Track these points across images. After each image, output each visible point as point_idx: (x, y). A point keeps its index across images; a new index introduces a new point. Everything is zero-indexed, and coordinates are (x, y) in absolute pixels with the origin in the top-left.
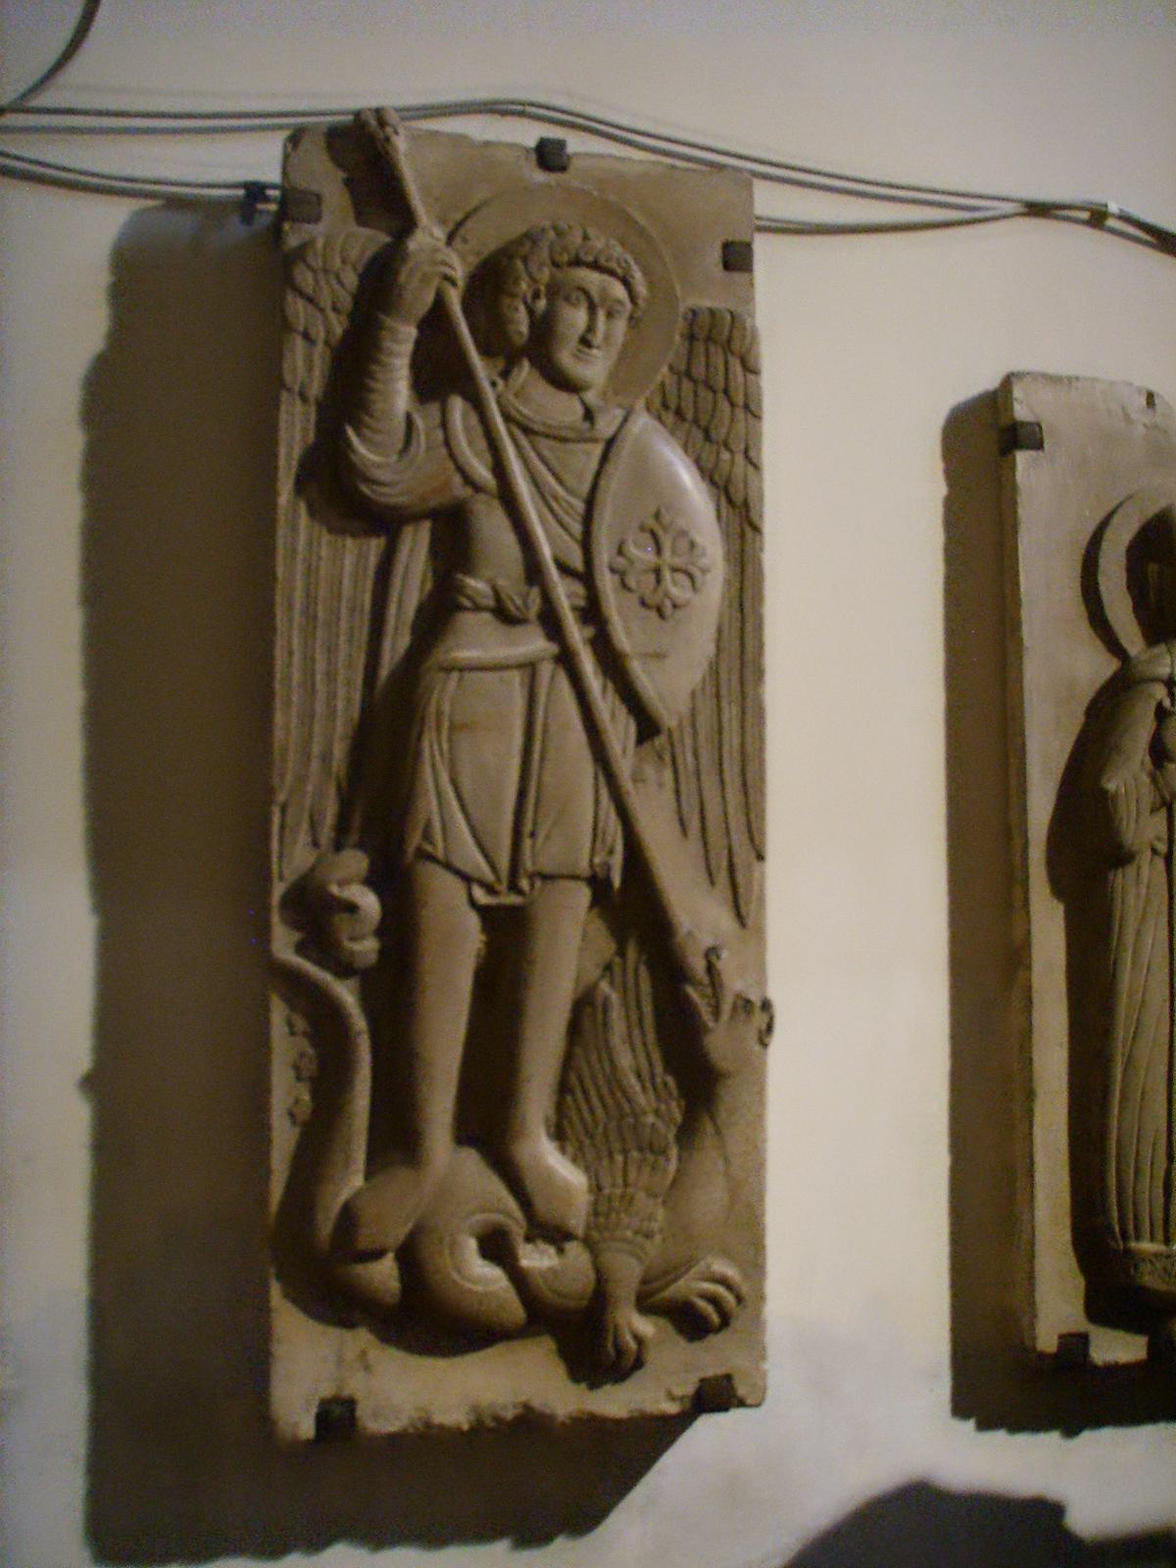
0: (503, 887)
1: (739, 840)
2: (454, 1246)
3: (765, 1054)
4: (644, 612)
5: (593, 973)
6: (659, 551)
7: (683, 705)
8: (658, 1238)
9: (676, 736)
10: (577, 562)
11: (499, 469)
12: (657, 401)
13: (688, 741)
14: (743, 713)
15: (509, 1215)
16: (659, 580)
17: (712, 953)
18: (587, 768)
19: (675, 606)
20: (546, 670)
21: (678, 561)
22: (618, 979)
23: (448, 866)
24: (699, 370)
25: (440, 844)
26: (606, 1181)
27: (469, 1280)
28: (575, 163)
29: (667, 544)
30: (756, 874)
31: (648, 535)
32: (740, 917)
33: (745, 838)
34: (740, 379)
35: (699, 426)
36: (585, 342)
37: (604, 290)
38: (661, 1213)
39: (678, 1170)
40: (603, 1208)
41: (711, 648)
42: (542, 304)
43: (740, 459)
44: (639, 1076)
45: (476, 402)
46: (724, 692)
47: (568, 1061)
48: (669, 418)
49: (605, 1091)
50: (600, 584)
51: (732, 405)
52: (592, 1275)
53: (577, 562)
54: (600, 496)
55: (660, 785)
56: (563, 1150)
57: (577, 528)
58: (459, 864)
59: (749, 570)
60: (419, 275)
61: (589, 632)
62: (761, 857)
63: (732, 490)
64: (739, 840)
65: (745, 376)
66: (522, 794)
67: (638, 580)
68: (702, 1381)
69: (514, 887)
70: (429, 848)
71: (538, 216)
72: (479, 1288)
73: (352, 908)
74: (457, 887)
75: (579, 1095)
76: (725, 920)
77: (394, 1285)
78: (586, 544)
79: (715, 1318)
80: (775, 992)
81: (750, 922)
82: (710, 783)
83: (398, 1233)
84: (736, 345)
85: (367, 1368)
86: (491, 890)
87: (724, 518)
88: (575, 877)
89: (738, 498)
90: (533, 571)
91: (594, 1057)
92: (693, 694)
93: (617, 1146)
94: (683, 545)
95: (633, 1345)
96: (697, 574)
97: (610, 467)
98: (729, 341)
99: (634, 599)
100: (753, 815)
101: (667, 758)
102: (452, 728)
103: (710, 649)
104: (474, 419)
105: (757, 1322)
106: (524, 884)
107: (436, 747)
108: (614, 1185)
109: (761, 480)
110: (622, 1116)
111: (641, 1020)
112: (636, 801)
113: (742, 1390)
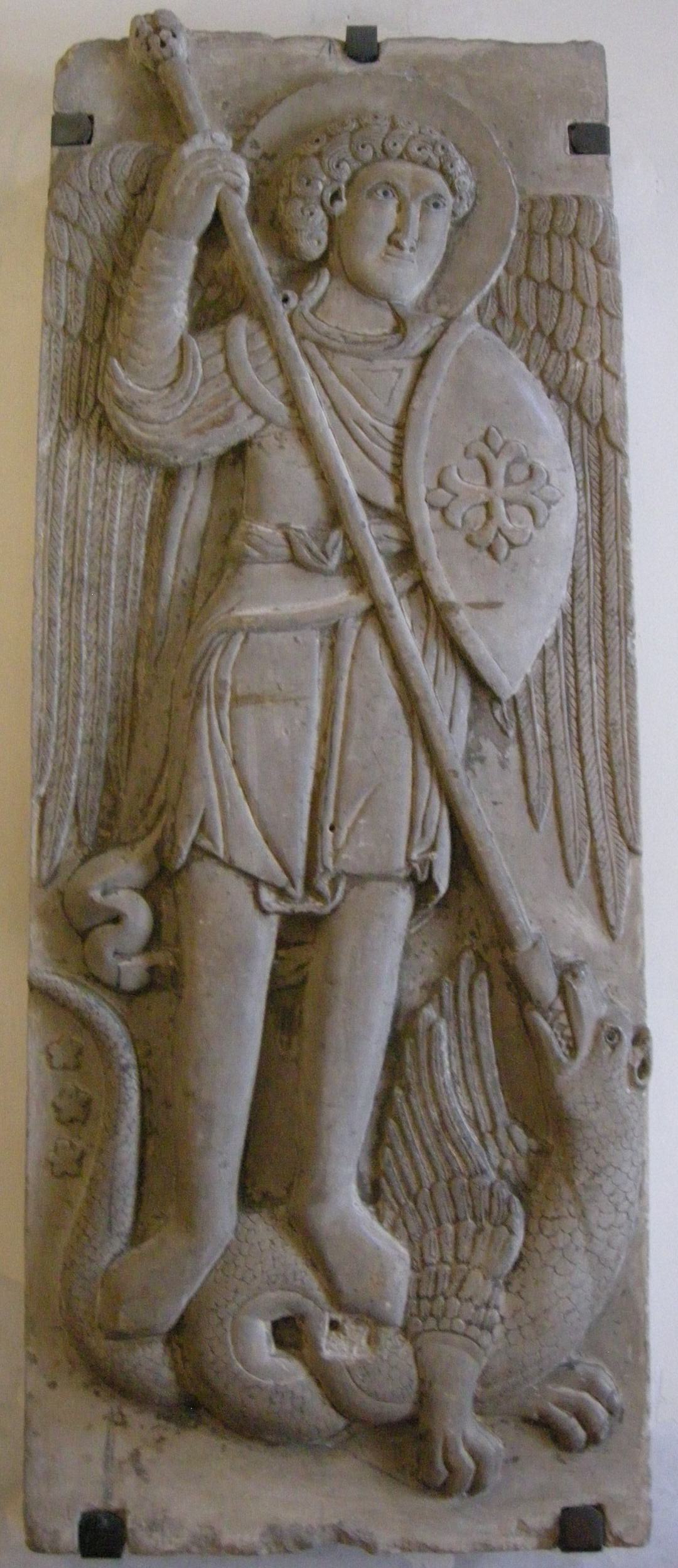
0: (298, 891)
1: (605, 830)
2: (239, 1332)
3: (643, 1100)
4: (474, 552)
5: (415, 997)
6: (489, 482)
7: (528, 664)
8: (498, 1331)
9: (522, 704)
10: (387, 498)
11: (293, 399)
12: (492, 311)
13: (537, 708)
14: (606, 674)
15: (307, 1295)
16: (489, 516)
17: (567, 973)
18: (404, 745)
19: (512, 545)
20: (351, 628)
21: (514, 491)
22: (448, 1002)
23: (229, 865)
24: (541, 270)
25: (221, 844)
26: (433, 1257)
27: (256, 1373)
28: (386, 53)
29: (499, 468)
30: (629, 872)
31: (476, 463)
32: (610, 930)
33: (612, 831)
34: (592, 274)
35: (543, 334)
36: (393, 241)
37: (416, 181)
38: (502, 1298)
39: (525, 1245)
40: (428, 1290)
41: (564, 594)
42: (341, 206)
43: (594, 370)
44: (477, 1125)
45: (264, 322)
46: (582, 649)
47: (385, 1103)
48: (508, 329)
49: (429, 1141)
50: (415, 523)
51: (584, 305)
52: (414, 1372)
53: (387, 498)
54: (414, 417)
55: (503, 764)
56: (379, 1216)
57: (387, 459)
58: (241, 861)
59: (610, 500)
60: (196, 184)
61: (405, 583)
62: (634, 851)
63: (586, 407)
64: (605, 830)
65: (598, 270)
66: (320, 777)
67: (462, 511)
68: (566, 1512)
69: (310, 887)
70: (205, 843)
71: (338, 102)
72: (270, 1383)
73: (116, 919)
74: (241, 889)
75: (401, 1151)
76: (590, 931)
77: (167, 1374)
78: (397, 476)
79: (581, 1434)
80: (653, 1023)
81: (621, 932)
82: (566, 760)
83: (169, 1314)
84: (585, 237)
85: (140, 1472)
86: (281, 893)
87: (577, 439)
88: (385, 877)
89: (595, 416)
90: (336, 517)
91: (416, 1101)
92: (543, 654)
93: (447, 1212)
94: (521, 472)
95: (470, 1462)
96: (541, 507)
97: (425, 384)
98: (575, 233)
99: (459, 541)
100: (622, 799)
101: (512, 733)
102: (236, 701)
103: (563, 595)
104: (262, 342)
105: (638, 1442)
106: (324, 884)
107: (215, 723)
108: (442, 1260)
109: (623, 390)
110: (454, 1176)
111: (478, 1056)
112: (466, 787)
113: (617, 1525)
